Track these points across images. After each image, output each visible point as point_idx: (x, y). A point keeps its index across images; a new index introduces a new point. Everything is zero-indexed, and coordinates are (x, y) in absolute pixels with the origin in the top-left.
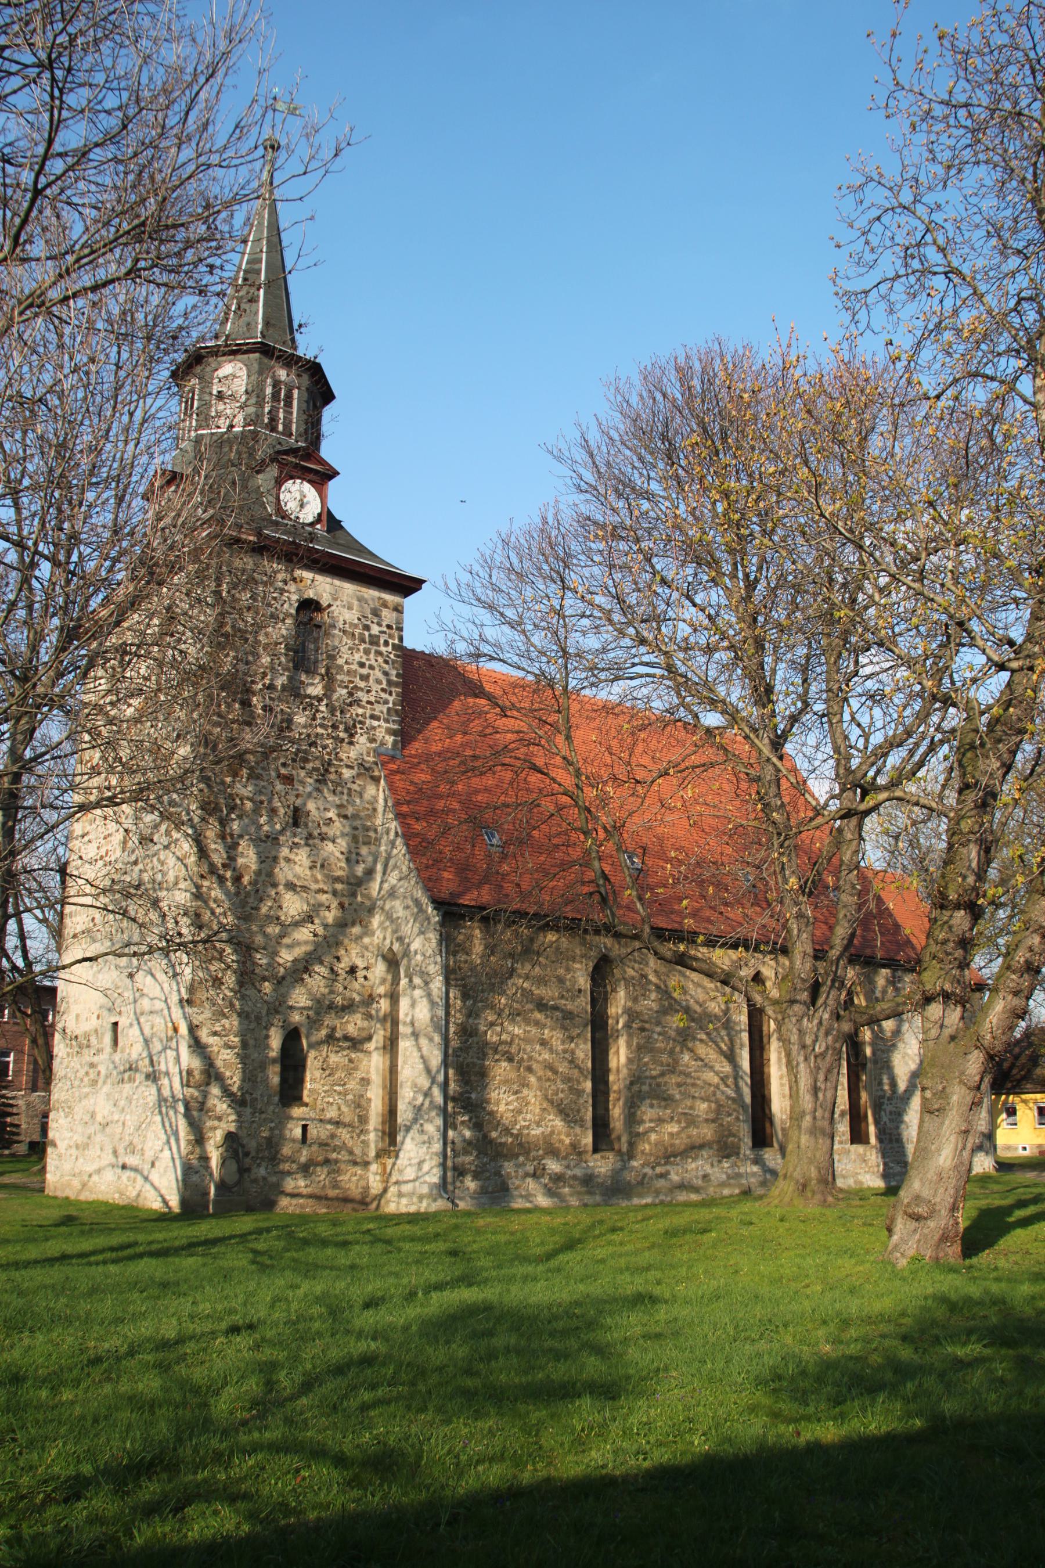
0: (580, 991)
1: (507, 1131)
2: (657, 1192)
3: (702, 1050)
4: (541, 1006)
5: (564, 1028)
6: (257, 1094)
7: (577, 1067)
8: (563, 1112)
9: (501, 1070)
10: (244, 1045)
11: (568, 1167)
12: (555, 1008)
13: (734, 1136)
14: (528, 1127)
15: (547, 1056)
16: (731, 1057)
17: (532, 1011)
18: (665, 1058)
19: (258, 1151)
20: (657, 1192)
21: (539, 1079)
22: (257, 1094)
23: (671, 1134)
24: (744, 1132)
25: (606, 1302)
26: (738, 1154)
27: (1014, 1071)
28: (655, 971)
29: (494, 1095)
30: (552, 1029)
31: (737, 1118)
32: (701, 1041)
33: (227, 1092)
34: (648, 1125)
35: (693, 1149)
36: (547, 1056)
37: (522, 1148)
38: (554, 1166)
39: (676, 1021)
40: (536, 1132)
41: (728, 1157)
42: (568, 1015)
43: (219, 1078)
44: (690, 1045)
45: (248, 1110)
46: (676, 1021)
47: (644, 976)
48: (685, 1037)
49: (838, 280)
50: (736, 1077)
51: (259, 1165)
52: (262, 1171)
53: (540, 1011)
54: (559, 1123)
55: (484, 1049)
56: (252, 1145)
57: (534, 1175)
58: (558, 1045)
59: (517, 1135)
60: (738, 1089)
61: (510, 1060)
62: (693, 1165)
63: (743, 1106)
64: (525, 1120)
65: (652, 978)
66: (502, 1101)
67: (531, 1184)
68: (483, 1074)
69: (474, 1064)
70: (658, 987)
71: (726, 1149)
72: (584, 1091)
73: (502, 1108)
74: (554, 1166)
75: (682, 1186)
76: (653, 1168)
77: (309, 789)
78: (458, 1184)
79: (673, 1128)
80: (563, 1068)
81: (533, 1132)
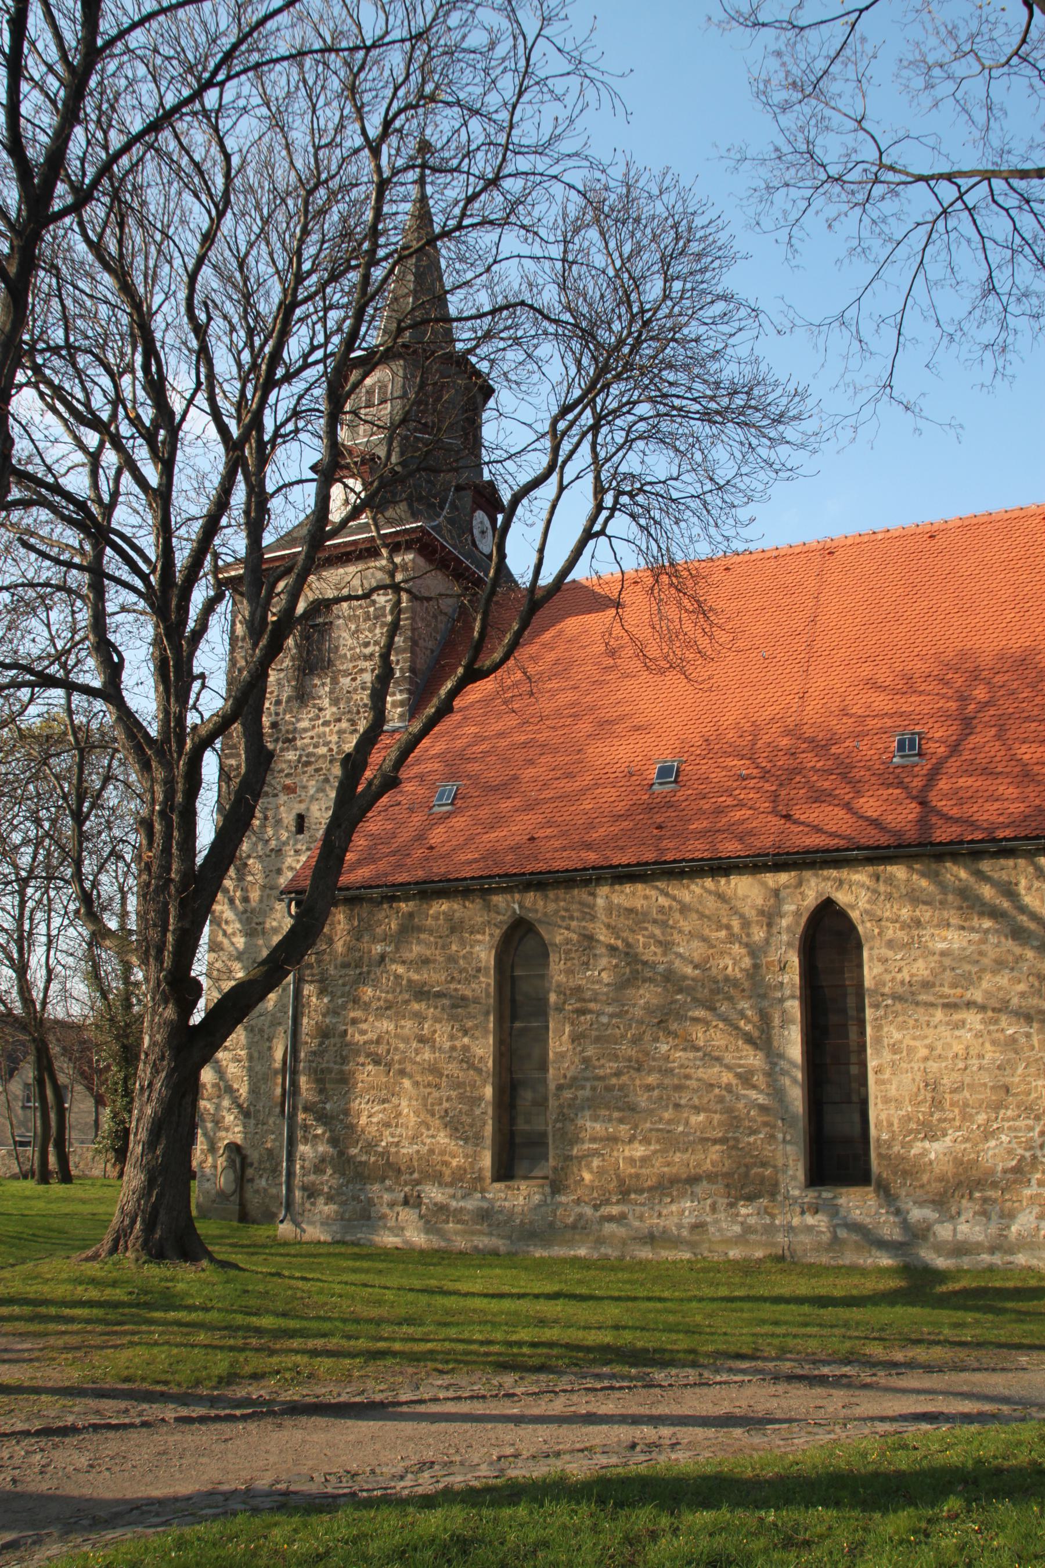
0: (479, 970)
1: (370, 1147)
2: (600, 1241)
3: (699, 1035)
4: (421, 993)
5: (453, 1018)
6: (260, 1106)
7: (472, 1066)
8: (454, 1126)
9: (367, 1074)
10: (250, 1058)
11: (453, 1196)
12: (439, 995)
13: (764, 1165)
15: (427, 1055)
16: (763, 1040)
17: (407, 1002)
18: (625, 1049)
19: (260, 1162)
20: (600, 1241)
21: (416, 1084)
22: (260, 1106)
23: (632, 1161)
24: (791, 1161)
26: (773, 1195)
28: (608, 926)
29: (355, 1105)
30: (437, 1020)
31: (772, 1137)
32: (696, 1020)
33: (235, 1101)
34: (586, 1146)
35: (669, 1187)
36: (427, 1055)
37: (390, 1169)
38: (434, 1194)
39: (646, 996)
41: (750, 1198)
42: (461, 1002)
43: (230, 1090)
44: (674, 1026)
45: (252, 1121)
46: (646, 996)
52: (263, 1183)
53: (419, 1000)
54: (443, 1139)
55: (346, 1052)
56: (254, 1155)
57: (406, 1202)
58: (442, 1039)
59: (382, 1155)
60: (778, 1093)
61: (377, 1062)
62: (674, 1208)
63: (787, 1119)
64: (393, 1135)
65: (603, 936)
66: (367, 1114)
67: (408, 1215)
68: (345, 1080)
69: (330, 1070)
70: (612, 949)
71: (747, 1183)
72: (481, 1098)
73: (363, 1120)
74: (434, 1194)
75: (651, 1239)
76: (596, 1207)
77: (312, 791)
78: (308, 1206)
80: (451, 1068)
81: (404, 1151)
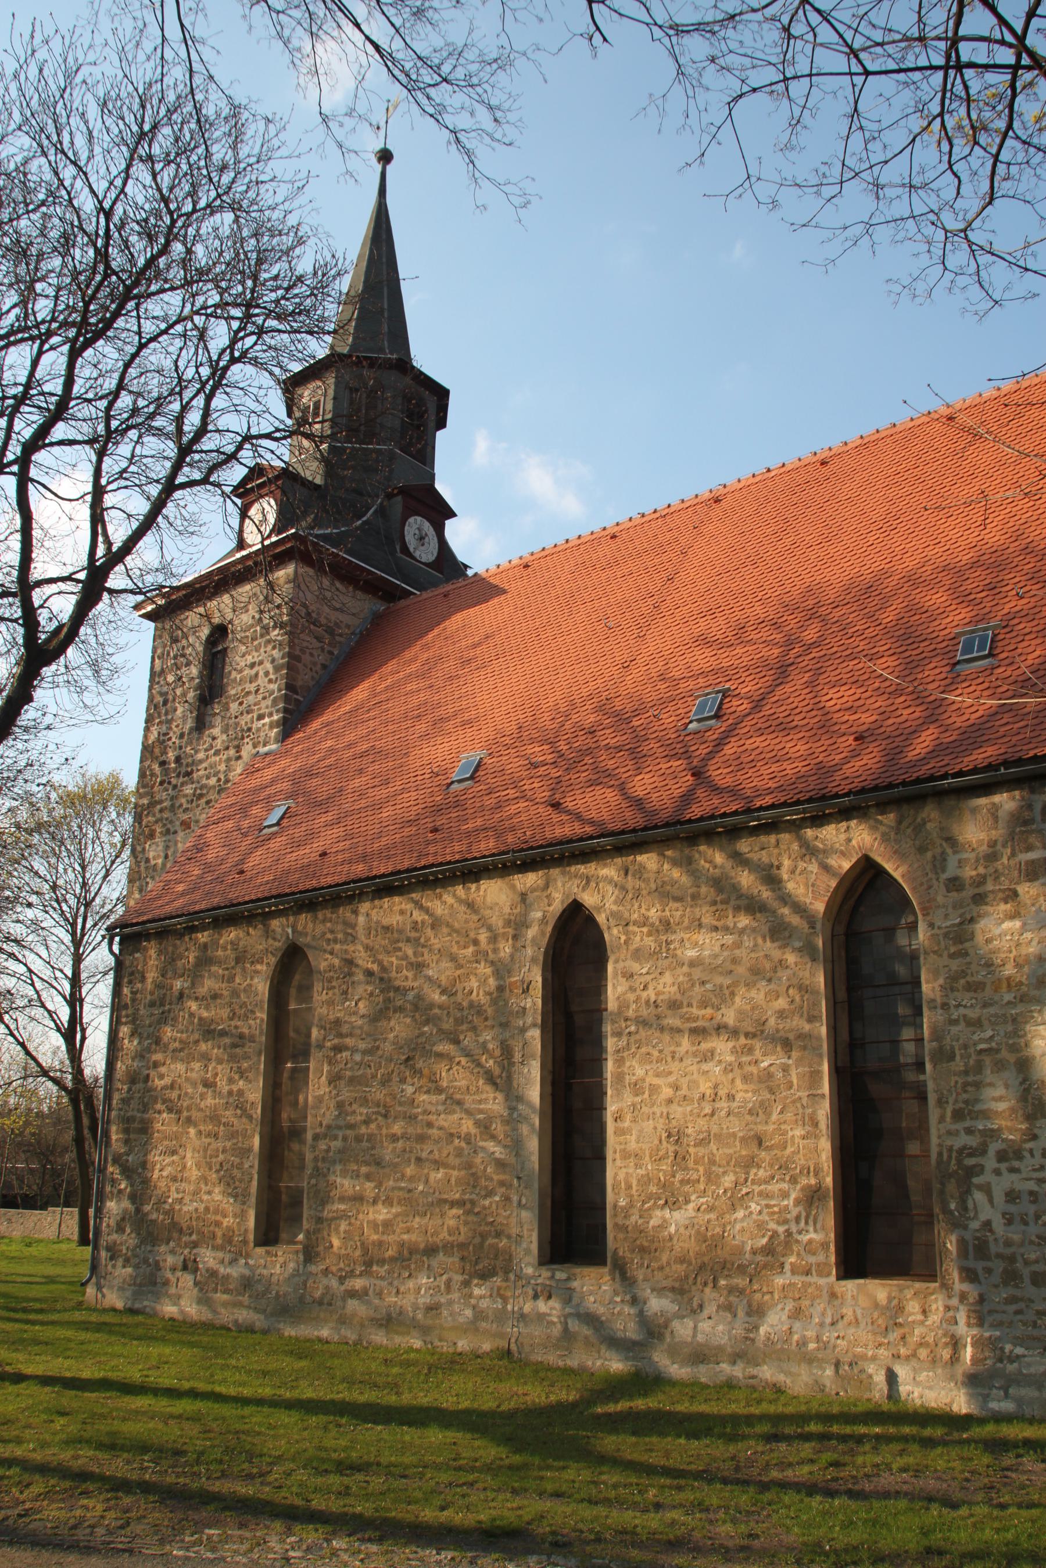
12: (223, 1033)
14: (180, 1201)
16: (503, 1081)
24: (524, 1228)
25: (687, 1386)
27: (1045, 1299)
35: (411, 1258)
39: (399, 1027)
40: (189, 1208)
41: (484, 1276)
42: (241, 1039)
46: (399, 1027)
47: (350, 962)
48: (413, 1056)
49: (926, 247)
50: (513, 1119)
51: (890, 1299)
70: (369, 973)
71: (483, 1260)
72: (250, 1150)
76: (342, 1280)
79: (382, 1213)
